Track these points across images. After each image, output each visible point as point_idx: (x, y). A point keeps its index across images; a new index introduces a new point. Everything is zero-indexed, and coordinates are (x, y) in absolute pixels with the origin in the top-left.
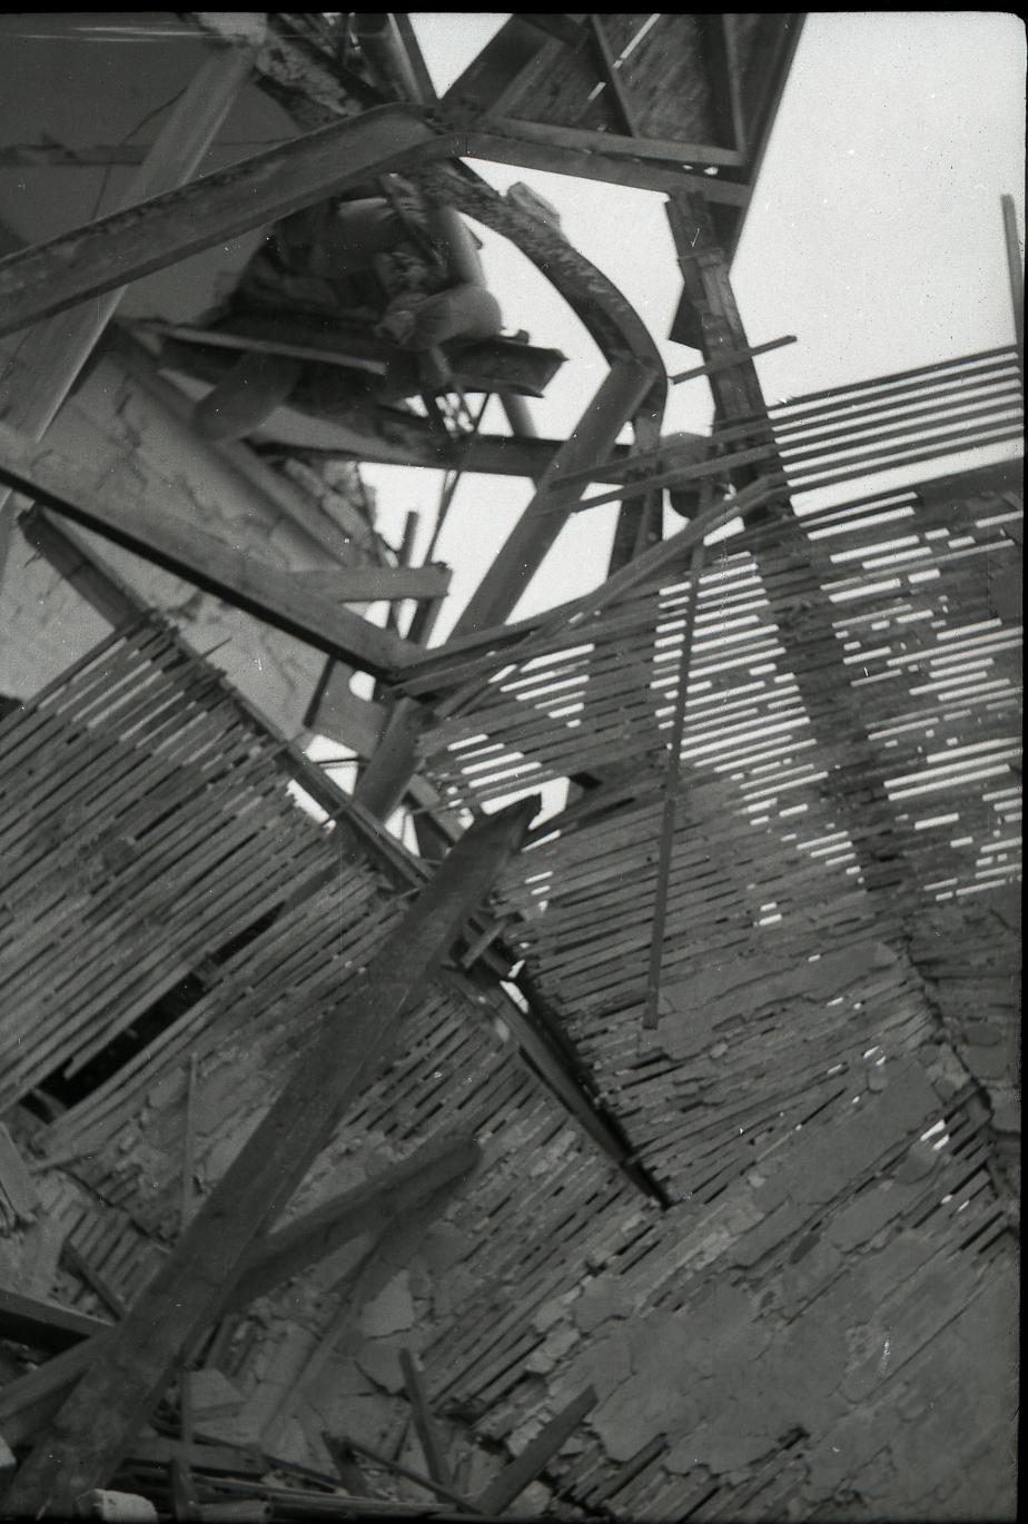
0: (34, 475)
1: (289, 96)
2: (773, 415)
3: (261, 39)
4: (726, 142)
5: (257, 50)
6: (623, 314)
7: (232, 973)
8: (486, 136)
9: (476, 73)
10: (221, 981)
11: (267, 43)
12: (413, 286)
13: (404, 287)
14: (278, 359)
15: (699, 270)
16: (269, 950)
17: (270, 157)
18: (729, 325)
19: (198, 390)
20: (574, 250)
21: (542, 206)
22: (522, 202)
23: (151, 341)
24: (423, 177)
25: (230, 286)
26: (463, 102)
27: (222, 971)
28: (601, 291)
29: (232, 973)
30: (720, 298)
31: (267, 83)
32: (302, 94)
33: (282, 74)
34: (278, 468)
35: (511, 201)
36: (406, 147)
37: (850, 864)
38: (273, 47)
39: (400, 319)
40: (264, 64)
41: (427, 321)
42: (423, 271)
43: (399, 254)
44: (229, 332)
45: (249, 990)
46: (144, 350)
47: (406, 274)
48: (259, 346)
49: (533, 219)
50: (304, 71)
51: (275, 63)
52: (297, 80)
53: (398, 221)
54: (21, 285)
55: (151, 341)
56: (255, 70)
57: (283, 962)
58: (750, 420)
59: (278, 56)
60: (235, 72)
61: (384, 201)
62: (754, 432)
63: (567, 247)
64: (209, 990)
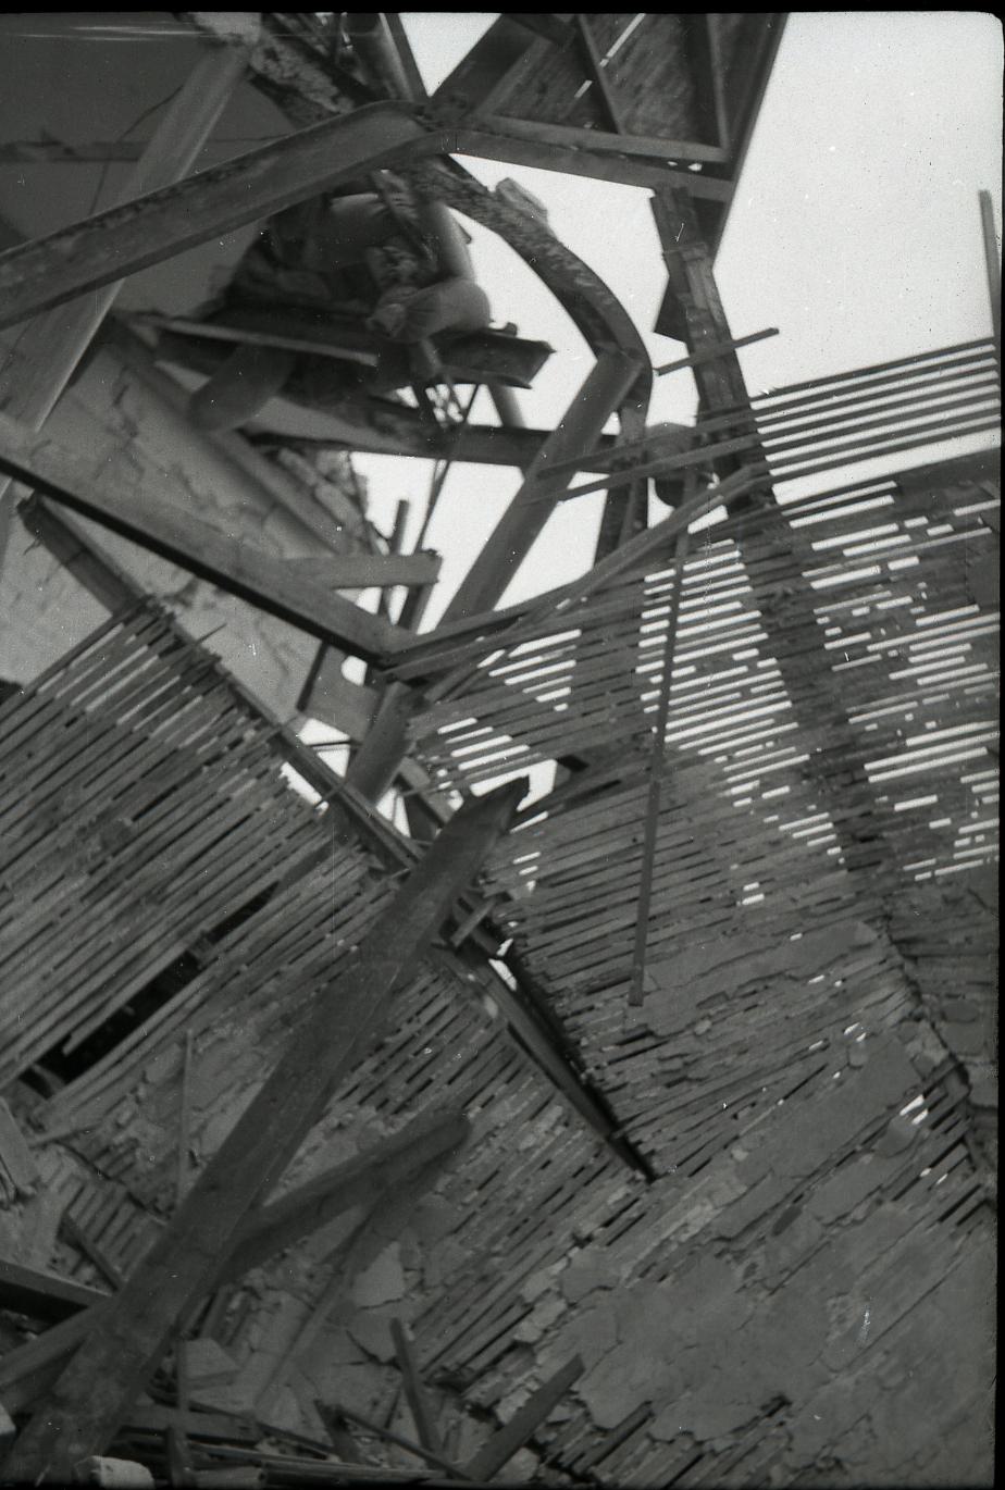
0: (33, 465)
1: (283, 94)
2: (755, 406)
3: (255, 38)
4: (710, 139)
5: (251, 49)
6: (609, 307)
7: (227, 951)
8: (475, 133)
9: (465, 71)
10: (216, 959)
11: (261, 42)
12: (404, 279)
13: (395, 280)
14: (272, 351)
15: (683, 264)
16: (263, 928)
17: (264, 153)
18: (712, 318)
19: (193, 381)
20: (561, 244)
21: (530, 202)
22: (510, 197)
23: (148, 334)
24: (414, 173)
25: (225, 279)
26: (453, 100)
27: (217, 949)
28: (588, 284)
29: (227, 951)
30: (704, 291)
31: (261, 82)
32: (295, 92)
33: (276, 72)
34: (272, 458)
35: (499, 196)
36: (396, 144)
37: (831, 845)
38: (267, 46)
39: (391, 311)
40: (258, 63)
41: (417, 314)
42: (414, 265)
43: (390, 248)
44: (224, 325)
45: (244, 968)
46: (141, 342)
47: (397, 268)
48: (254, 338)
49: (521, 214)
50: (297, 69)
51: (269, 61)
52: (290, 78)
53: (389, 216)
54: (20, 278)
55: (148, 334)
56: (249, 68)
57: (277, 940)
58: (733, 410)
59: (272, 55)
60: (230, 70)
61: (375, 196)
62: (737, 422)
63: (554, 241)
64: (205, 968)
